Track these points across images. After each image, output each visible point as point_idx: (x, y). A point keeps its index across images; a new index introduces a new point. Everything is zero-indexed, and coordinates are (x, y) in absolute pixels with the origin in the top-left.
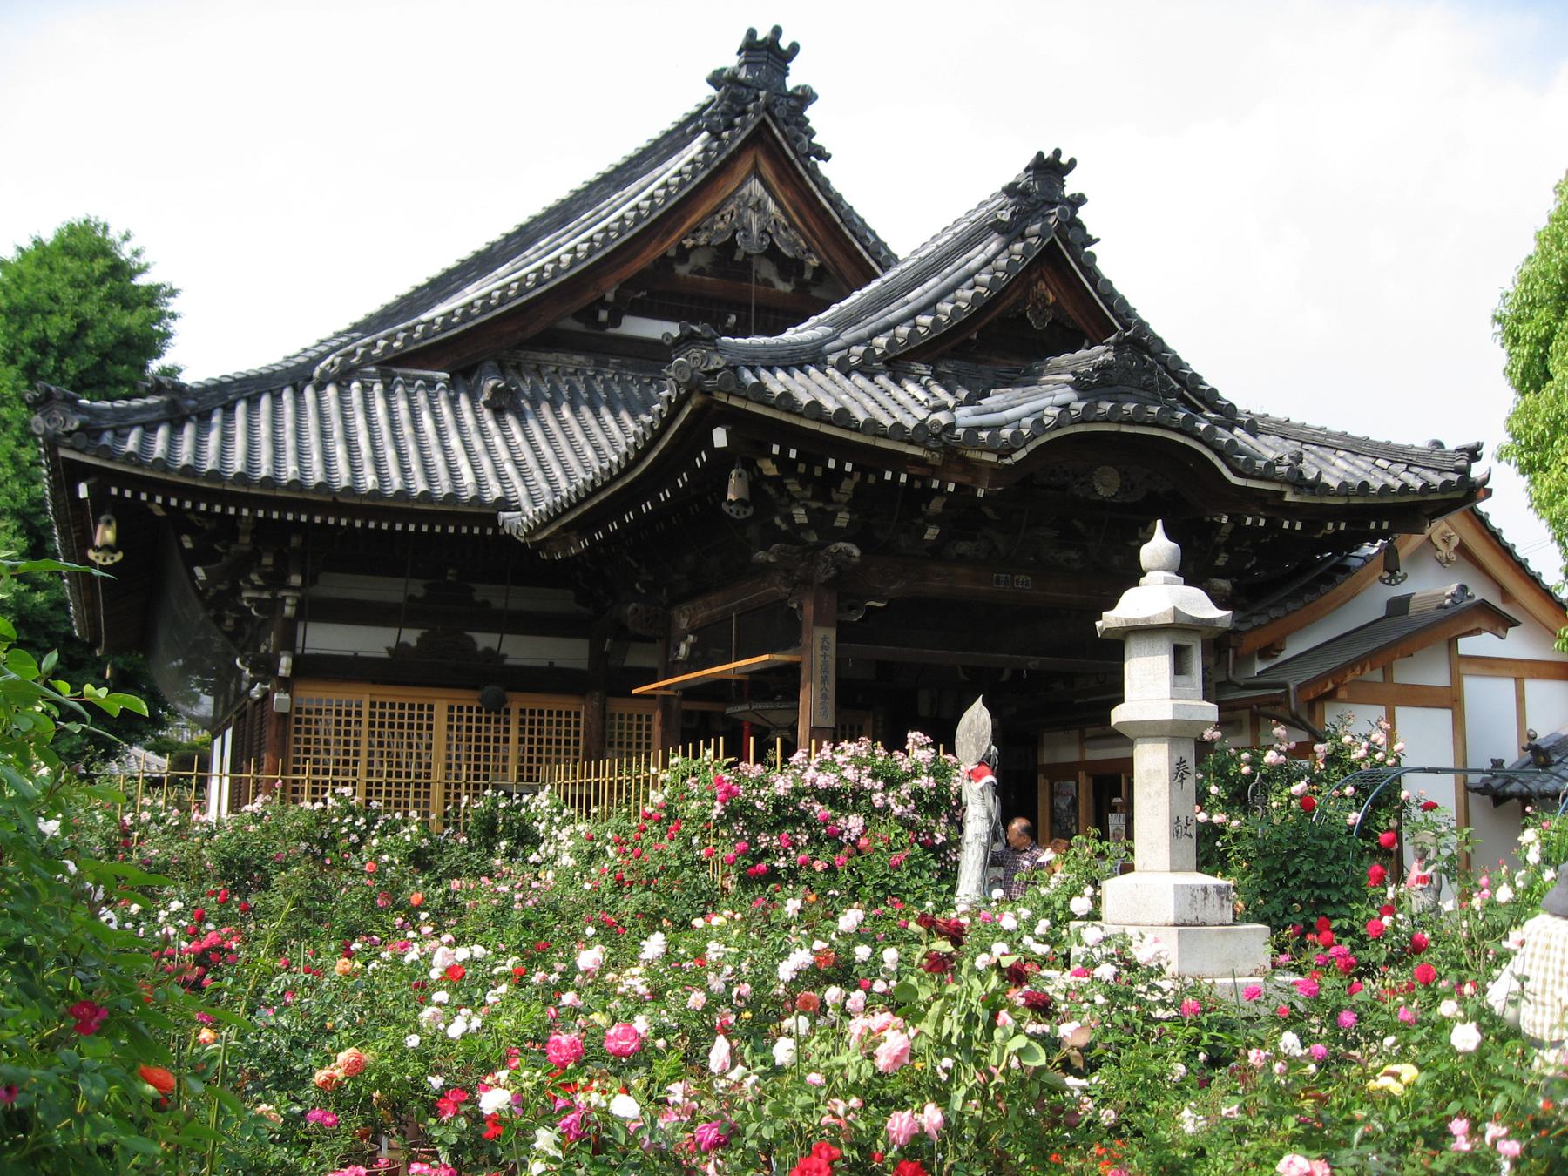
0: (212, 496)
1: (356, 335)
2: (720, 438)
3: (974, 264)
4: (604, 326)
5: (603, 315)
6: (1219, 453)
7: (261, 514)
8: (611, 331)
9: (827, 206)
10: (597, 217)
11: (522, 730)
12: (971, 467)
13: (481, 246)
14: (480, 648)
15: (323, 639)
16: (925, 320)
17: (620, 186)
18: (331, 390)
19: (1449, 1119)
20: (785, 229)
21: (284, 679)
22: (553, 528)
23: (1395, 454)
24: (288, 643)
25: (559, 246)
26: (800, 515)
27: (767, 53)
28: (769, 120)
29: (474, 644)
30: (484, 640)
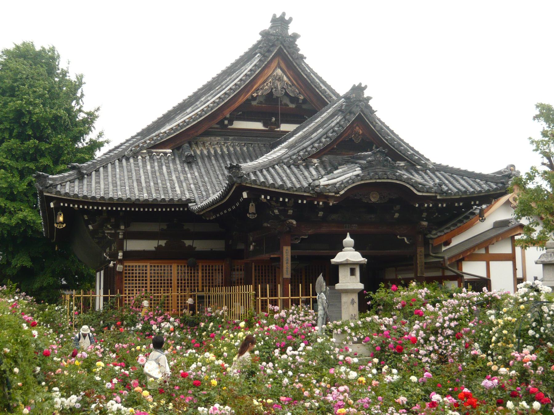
0: (93, 204)
1: (139, 137)
2: (245, 195)
3: (333, 124)
4: (227, 125)
5: (226, 122)
6: (412, 186)
7: (110, 208)
8: (229, 127)
9: (305, 77)
10: (221, 89)
11: (203, 273)
12: (327, 197)
13: (181, 101)
14: (187, 245)
15: (132, 245)
16: (316, 145)
17: (230, 75)
18: (131, 160)
19: (212, 379)
20: (291, 86)
21: (120, 260)
22: (204, 211)
23: (481, 176)
24: (121, 247)
25: (208, 101)
26: (276, 212)
27: (281, 22)
28: (282, 47)
29: (185, 244)
30: (188, 243)
